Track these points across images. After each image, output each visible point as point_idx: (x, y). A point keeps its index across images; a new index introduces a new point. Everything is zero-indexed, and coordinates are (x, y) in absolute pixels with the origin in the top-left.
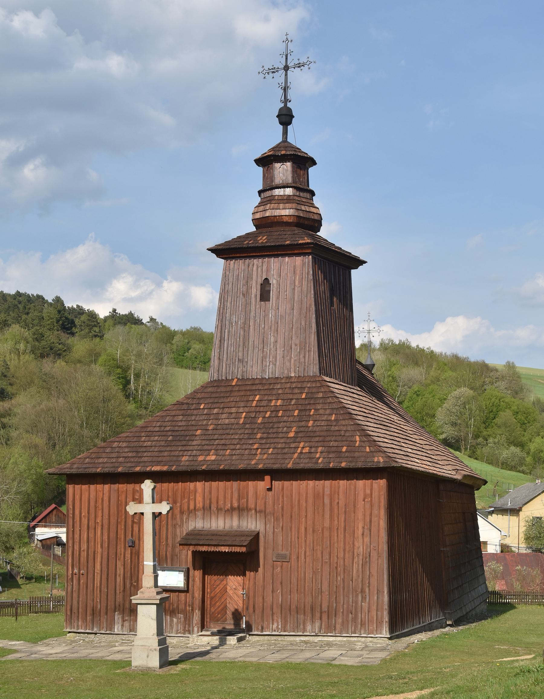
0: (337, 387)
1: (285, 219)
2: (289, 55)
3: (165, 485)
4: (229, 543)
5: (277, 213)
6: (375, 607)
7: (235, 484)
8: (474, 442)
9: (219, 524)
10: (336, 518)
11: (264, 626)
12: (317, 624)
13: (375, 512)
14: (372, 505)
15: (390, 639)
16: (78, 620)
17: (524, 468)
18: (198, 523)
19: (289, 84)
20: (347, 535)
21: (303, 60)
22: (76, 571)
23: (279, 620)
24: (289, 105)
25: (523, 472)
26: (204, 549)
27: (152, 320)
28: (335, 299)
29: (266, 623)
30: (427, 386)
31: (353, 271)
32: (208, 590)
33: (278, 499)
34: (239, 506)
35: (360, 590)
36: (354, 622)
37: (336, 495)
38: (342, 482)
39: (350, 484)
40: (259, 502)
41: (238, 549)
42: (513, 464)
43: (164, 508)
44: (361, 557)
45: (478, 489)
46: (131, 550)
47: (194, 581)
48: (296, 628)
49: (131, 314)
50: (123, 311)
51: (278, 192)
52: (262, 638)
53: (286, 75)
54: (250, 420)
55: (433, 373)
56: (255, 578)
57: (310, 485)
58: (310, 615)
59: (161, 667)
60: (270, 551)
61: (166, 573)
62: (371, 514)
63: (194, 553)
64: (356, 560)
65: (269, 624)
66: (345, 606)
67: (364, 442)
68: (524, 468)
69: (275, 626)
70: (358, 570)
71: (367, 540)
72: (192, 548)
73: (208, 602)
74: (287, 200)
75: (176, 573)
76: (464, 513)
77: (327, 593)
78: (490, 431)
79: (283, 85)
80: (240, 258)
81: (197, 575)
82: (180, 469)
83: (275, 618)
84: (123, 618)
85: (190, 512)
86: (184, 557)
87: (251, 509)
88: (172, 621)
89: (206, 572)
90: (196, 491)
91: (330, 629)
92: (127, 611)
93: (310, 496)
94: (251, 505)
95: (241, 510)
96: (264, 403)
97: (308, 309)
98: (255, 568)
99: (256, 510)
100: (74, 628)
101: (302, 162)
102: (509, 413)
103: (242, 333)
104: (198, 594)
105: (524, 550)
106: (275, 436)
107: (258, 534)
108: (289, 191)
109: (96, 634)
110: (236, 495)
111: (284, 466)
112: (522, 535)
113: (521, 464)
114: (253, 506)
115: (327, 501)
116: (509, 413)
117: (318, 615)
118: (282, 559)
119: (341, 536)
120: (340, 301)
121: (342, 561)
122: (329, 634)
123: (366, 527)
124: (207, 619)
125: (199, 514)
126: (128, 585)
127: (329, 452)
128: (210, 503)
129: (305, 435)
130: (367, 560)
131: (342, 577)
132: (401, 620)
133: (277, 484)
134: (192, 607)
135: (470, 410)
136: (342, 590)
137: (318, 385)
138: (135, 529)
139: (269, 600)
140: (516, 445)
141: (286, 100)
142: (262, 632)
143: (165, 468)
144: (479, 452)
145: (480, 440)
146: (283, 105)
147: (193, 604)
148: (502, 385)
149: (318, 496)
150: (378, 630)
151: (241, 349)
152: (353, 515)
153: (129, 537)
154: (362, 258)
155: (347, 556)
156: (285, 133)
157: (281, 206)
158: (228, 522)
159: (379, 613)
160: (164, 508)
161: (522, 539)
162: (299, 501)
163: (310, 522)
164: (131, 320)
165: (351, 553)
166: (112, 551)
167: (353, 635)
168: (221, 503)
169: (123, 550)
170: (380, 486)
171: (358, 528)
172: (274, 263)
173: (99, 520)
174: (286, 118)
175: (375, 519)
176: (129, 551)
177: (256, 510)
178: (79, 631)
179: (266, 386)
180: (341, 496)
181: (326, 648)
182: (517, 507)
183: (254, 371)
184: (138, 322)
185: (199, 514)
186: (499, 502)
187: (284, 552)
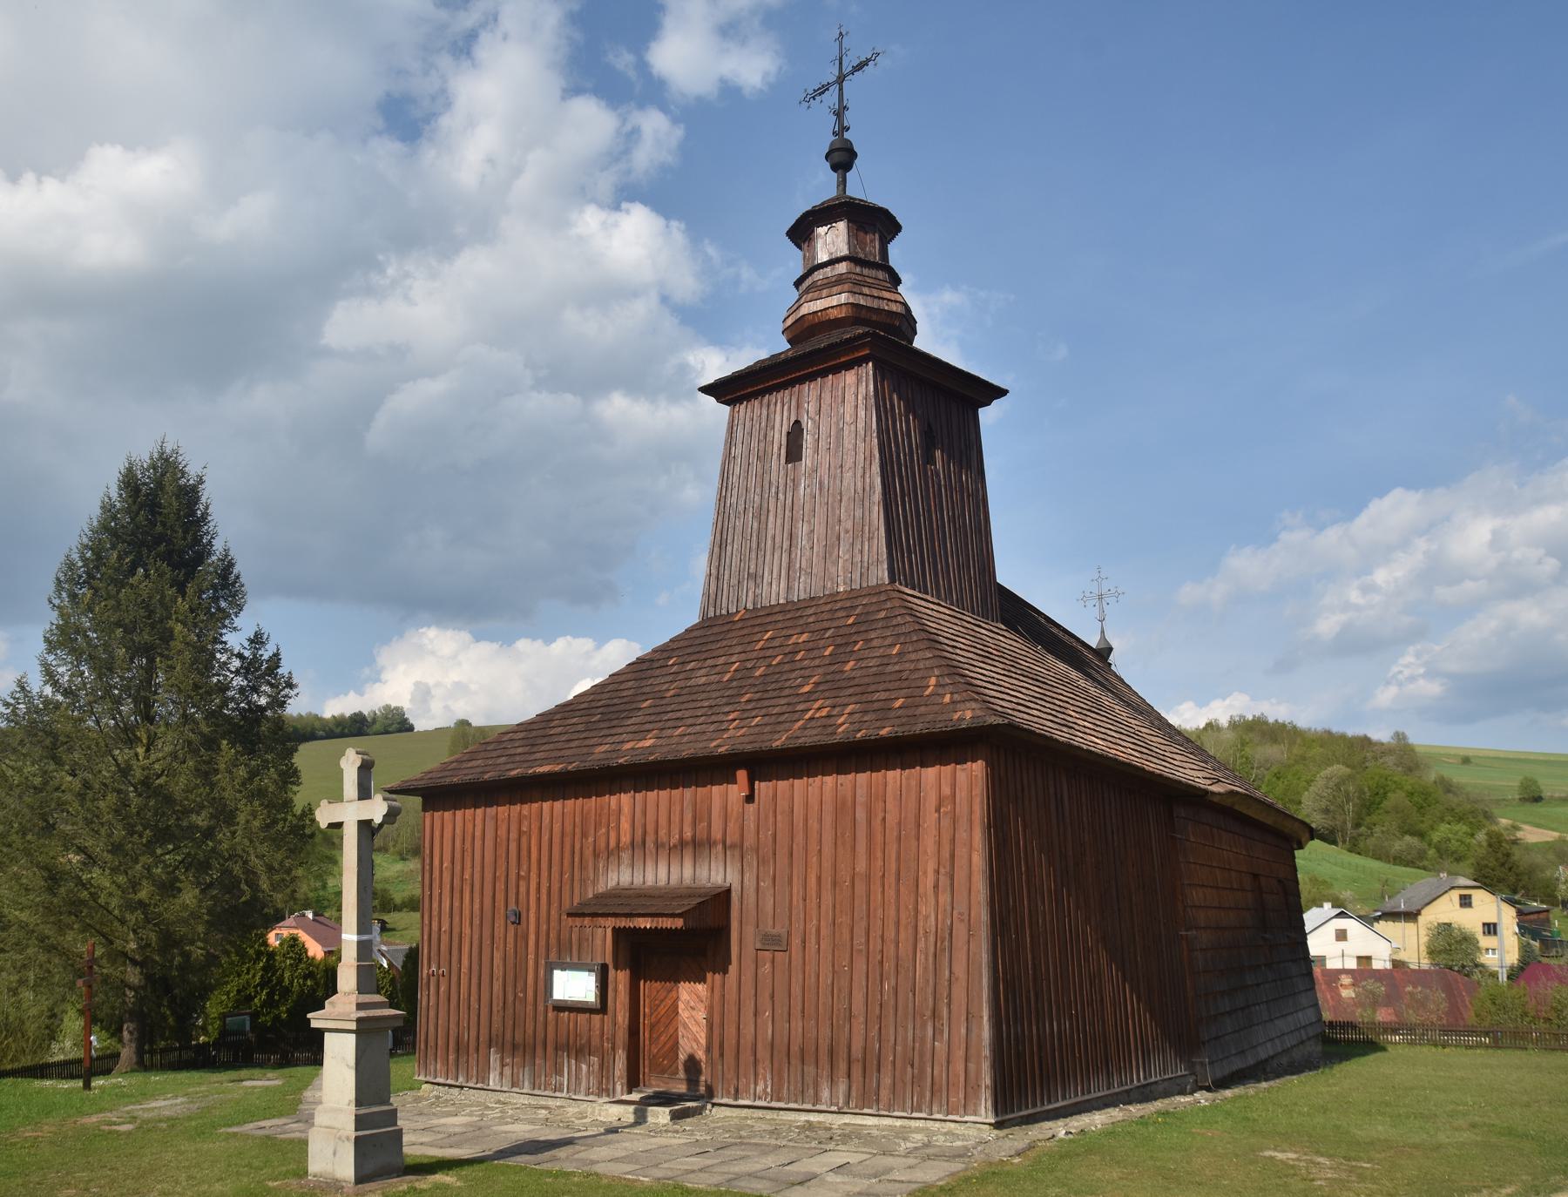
0: (937, 614)
1: (834, 314)
3: (570, 803)
4: (652, 910)
6: (961, 1053)
8: (1355, 833)
9: (658, 874)
10: (879, 854)
12: (842, 1087)
13: (962, 835)
15: (998, 1125)
17: (1426, 863)
18: (620, 876)
20: (902, 889)
23: (768, 1077)
24: (846, 135)
25: (1424, 868)
26: (646, 923)
28: (938, 454)
29: (743, 1081)
30: (1289, 766)
31: (919, 343)
32: (645, 1009)
33: (767, 817)
34: (694, 836)
35: (929, 1013)
36: (920, 1087)
37: (881, 804)
39: (908, 779)
40: (731, 825)
41: (667, 923)
44: (932, 939)
45: (1301, 847)
47: (616, 991)
48: (802, 1095)
52: (737, 1112)
53: (841, 89)
54: (744, 673)
55: (1296, 750)
57: (827, 785)
58: (827, 1067)
59: (360, 1179)
60: (750, 930)
62: (953, 840)
64: (921, 945)
65: (748, 1084)
66: (899, 1048)
67: (943, 686)
68: (1426, 863)
70: (926, 968)
71: (944, 898)
72: (610, 923)
73: (644, 1035)
76: (1255, 876)
77: (862, 1019)
78: (1374, 818)
81: (620, 979)
83: (761, 1071)
84: (502, 1059)
86: (598, 942)
88: (578, 1069)
89: (638, 975)
91: (867, 1099)
92: (508, 1046)
93: (828, 807)
94: (717, 834)
95: (698, 846)
96: (776, 643)
101: (873, 223)
102: (1400, 795)
103: (756, 525)
104: (622, 1018)
105: (1425, 964)
106: (775, 694)
107: (729, 891)
108: (842, 268)
110: (688, 817)
111: (765, 746)
112: (1423, 948)
115: (861, 815)
116: (1400, 795)
117: (842, 1066)
118: (774, 943)
121: (892, 947)
122: (866, 1111)
123: (942, 870)
124: (645, 1068)
125: (625, 856)
126: (510, 998)
127: (865, 712)
128: (645, 833)
129: (833, 686)
130: (944, 941)
131: (893, 982)
132: (1021, 1087)
133: (762, 787)
134: (614, 1044)
135: (1347, 793)
136: (892, 1011)
137: (883, 598)
139: (748, 1031)
140: (1412, 834)
142: (736, 1099)
143: (557, 768)
144: (1362, 845)
145: (1363, 829)
147: (614, 1036)
148: (1390, 760)
149: (843, 808)
150: (968, 1106)
151: (753, 555)
152: (914, 843)
153: (512, 906)
155: (902, 936)
156: (843, 183)
158: (703, 873)
159: (972, 1066)
161: (1424, 953)
162: (806, 820)
163: (827, 865)
165: (911, 931)
167: (915, 1115)
168: (662, 833)
170: (971, 775)
171: (925, 873)
173: (467, 876)
174: (842, 158)
175: (961, 852)
181: (831, 1146)
182: (1413, 909)
185: (625, 856)
186: (1389, 905)
187: (774, 932)
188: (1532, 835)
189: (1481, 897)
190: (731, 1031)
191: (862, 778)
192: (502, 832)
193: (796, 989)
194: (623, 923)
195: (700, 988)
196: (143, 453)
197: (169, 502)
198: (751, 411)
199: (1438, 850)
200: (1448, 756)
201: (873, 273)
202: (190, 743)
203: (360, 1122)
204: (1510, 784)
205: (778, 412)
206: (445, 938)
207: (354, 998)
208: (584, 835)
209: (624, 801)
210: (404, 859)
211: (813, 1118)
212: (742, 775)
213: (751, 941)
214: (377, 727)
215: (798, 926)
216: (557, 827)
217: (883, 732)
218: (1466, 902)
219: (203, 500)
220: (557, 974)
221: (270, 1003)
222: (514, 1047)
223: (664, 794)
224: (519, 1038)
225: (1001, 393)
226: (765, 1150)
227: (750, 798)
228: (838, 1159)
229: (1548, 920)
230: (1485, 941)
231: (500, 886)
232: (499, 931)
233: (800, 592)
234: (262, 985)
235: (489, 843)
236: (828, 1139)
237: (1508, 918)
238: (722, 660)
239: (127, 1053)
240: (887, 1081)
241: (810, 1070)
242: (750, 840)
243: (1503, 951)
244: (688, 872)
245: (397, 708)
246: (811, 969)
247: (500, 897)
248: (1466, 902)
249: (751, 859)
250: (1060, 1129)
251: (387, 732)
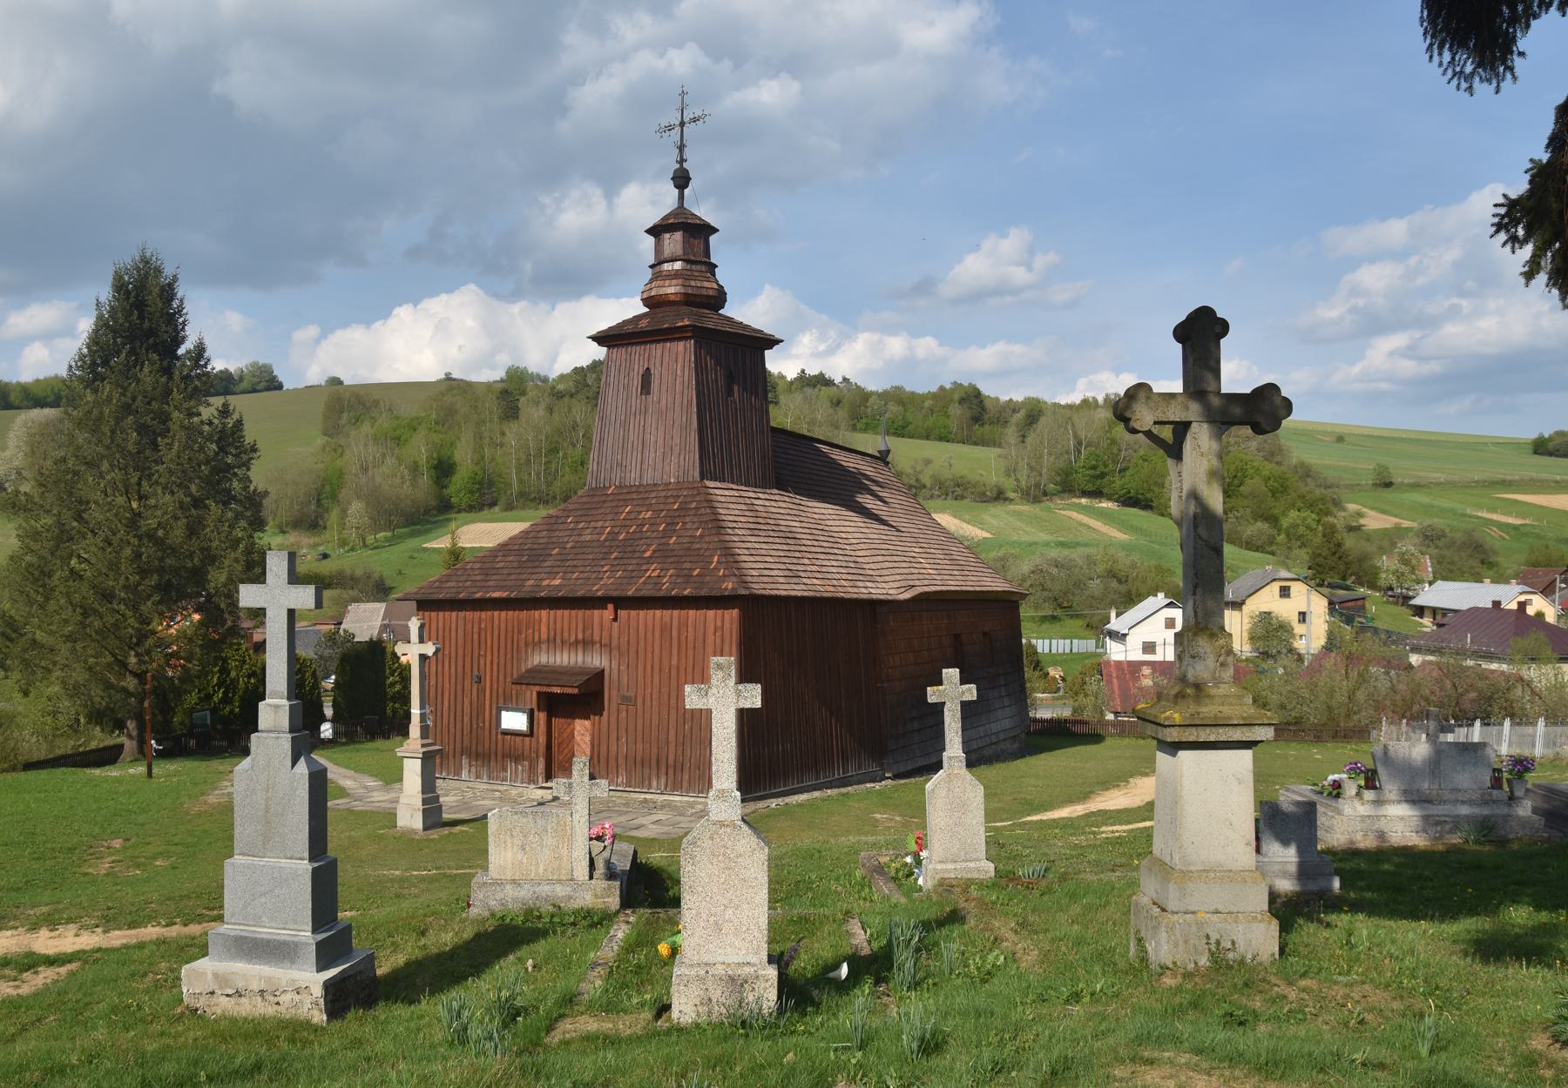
1: (672, 298)
5: (663, 291)
9: (563, 659)
12: (663, 780)
18: (541, 658)
21: (698, 113)
24: (685, 165)
25: (1273, 554)
26: (557, 690)
27: (845, 379)
32: (555, 734)
42: (1259, 543)
49: (821, 375)
50: (812, 371)
51: (667, 267)
54: (613, 535)
59: (425, 829)
60: (614, 693)
63: (539, 694)
68: (1274, 548)
72: (537, 688)
73: (555, 749)
74: (675, 275)
80: (622, 345)
81: (541, 717)
82: (522, 595)
85: (534, 644)
91: (676, 787)
94: (596, 637)
95: (586, 644)
97: (690, 402)
101: (698, 232)
104: (542, 739)
108: (678, 265)
111: (623, 594)
112: (1245, 635)
113: (1271, 543)
115: (675, 634)
117: (663, 769)
118: (627, 700)
120: (745, 389)
124: (555, 767)
125: (544, 646)
129: (663, 554)
133: (622, 613)
139: (614, 749)
141: (682, 161)
143: (505, 595)
149: (666, 629)
154: (778, 336)
156: (681, 197)
158: (588, 659)
160: (429, 649)
163: (657, 660)
164: (822, 381)
166: (459, 687)
172: (657, 350)
174: (682, 180)
179: (637, 494)
180: (690, 629)
183: (633, 477)
184: (829, 383)
185: (544, 646)
188: (1374, 521)
189: (1298, 589)
190: (604, 748)
191: (676, 612)
192: (469, 627)
193: (640, 727)
194: (544, 689)
195: (587, 723)
196: (128, 257)
197: (153, 298)
198: (620, 353)
199: (1288, 536)
200: (1324, 433)
201: (699, 267)
202: (181, 503)
203: (424, 802)
204: (1365, 466)
205: (639, 357)
206: (433, 690)
207: (419, 742)
208: (519, 632)
209: (543, 614)
210: (283, 532)
211: (648, 796)
212: (610, 606)
213: (615, 699)
214: (245, 385)
215: (640, 692)
216: (503, 627)
217: (686, 593)
218: (1285, 592)
219: (179, 295)
220: (504, 714)
221: (226, 700)
222: (477, 755)
223: (566, 612)
224: (480, 749)
225: (778, 342)
226: (620, 813)
227: (615, 619)
228: (656, 817)
229: (1363, 607)
230: (1299, 629)
231: (468, 660)
232: (467, 687)
233: (648, 479)
234: (219, 685)
235: (461, 633)
236: (655, 806)
237: (1318, 606)
238: (600, 524)
239: (129, 745)
240: (686, 777)
241: (646, 771)
242: (614, 643)
243: (1312, 637)
244: (580, 658)
245: (265, 366)
246: (647, 716)
247: (468, 665)
248: (1285, 592)
249: (615, 652)
250: (773, 803)
251: (255, 391)
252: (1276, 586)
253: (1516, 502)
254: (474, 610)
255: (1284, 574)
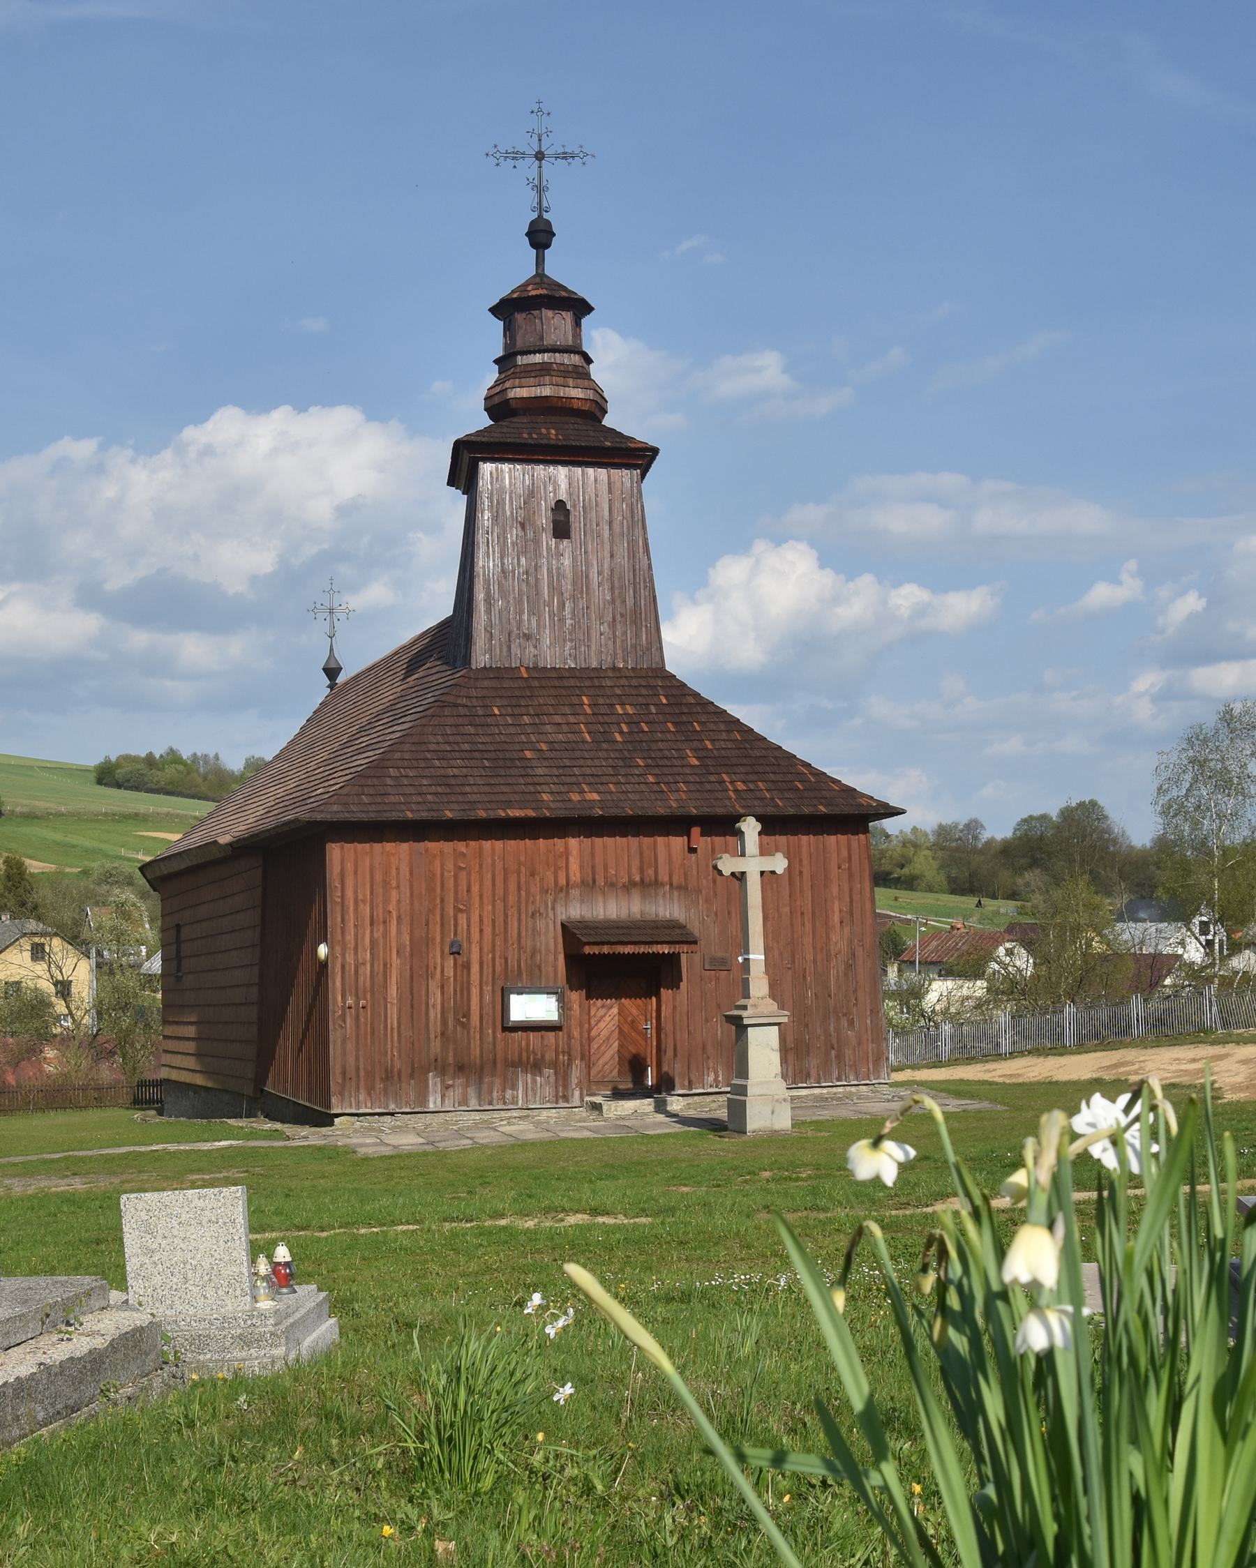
2: (544, 137)
5: (562, 392)
7: (633, 842)
9: (610, 909)
11: (693, 1078)
14: (851, 876)
16: (358, 1089)
19: (545, 183)
22: (350, 1001)
24: (546, 216)
26: (628, 949)
34: (642, 880)
38: (804, 838)
43: (779, 864)
46: (455, 960)
51: (520, 360)
56: (674, 999)
61: (524, 998)
69: (711, 1078)
75: (543, 998)
79: (536, 182)
84: (443, 1082)
87: (663, 885)
88: (534, 1082)
90: (567, 853)
95: (647, 886)
98: (675, 983)
99: (671, 885)
100: (351, 1107)
109: (392, 1114)
114: (666, 879)
119: (808, 926)
125: (575, 893)
138: (460, 922)
141: (540, 208)
142: (690, 1088)
143: (532, 813)
146: (535, 215)
156: (540, 261)
157: (570, 382)
160: (779, 864)
169: (439, 961)
174: (540, 236)
175: (856, 897)
176: (450, 961)
177: (671, 885)
178: (361, 1111)
180: (806, 862)
252: (26, 944)
253: (147, 837)
254: (448, 839)
255: (32, 925)
